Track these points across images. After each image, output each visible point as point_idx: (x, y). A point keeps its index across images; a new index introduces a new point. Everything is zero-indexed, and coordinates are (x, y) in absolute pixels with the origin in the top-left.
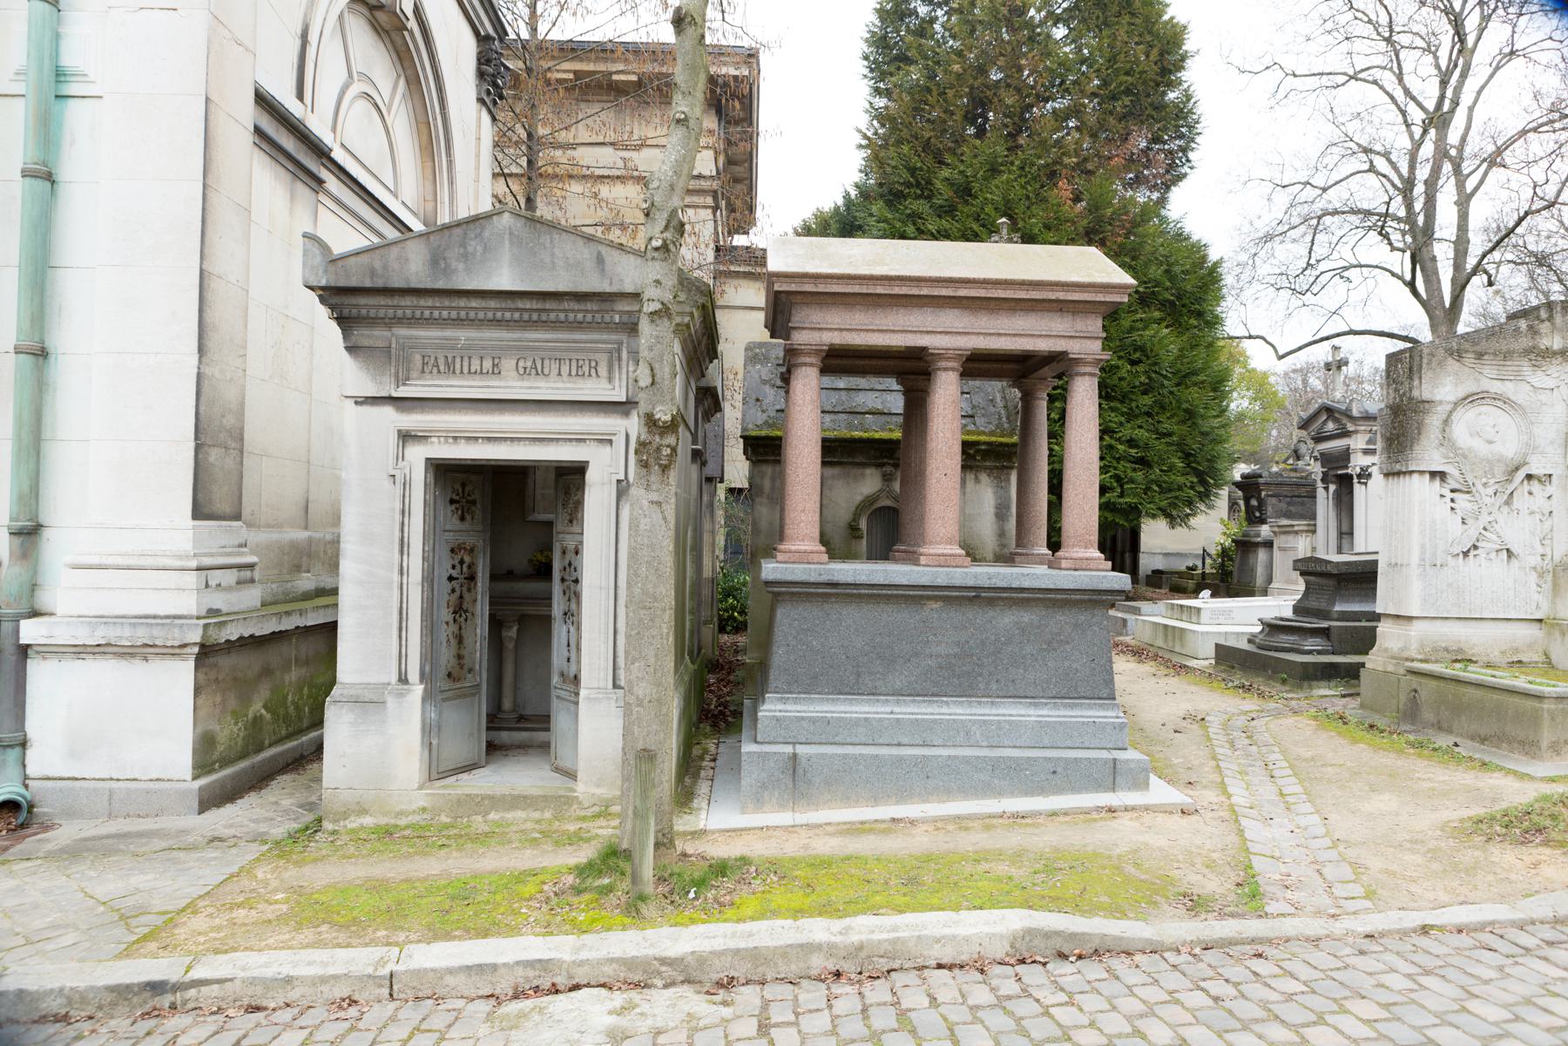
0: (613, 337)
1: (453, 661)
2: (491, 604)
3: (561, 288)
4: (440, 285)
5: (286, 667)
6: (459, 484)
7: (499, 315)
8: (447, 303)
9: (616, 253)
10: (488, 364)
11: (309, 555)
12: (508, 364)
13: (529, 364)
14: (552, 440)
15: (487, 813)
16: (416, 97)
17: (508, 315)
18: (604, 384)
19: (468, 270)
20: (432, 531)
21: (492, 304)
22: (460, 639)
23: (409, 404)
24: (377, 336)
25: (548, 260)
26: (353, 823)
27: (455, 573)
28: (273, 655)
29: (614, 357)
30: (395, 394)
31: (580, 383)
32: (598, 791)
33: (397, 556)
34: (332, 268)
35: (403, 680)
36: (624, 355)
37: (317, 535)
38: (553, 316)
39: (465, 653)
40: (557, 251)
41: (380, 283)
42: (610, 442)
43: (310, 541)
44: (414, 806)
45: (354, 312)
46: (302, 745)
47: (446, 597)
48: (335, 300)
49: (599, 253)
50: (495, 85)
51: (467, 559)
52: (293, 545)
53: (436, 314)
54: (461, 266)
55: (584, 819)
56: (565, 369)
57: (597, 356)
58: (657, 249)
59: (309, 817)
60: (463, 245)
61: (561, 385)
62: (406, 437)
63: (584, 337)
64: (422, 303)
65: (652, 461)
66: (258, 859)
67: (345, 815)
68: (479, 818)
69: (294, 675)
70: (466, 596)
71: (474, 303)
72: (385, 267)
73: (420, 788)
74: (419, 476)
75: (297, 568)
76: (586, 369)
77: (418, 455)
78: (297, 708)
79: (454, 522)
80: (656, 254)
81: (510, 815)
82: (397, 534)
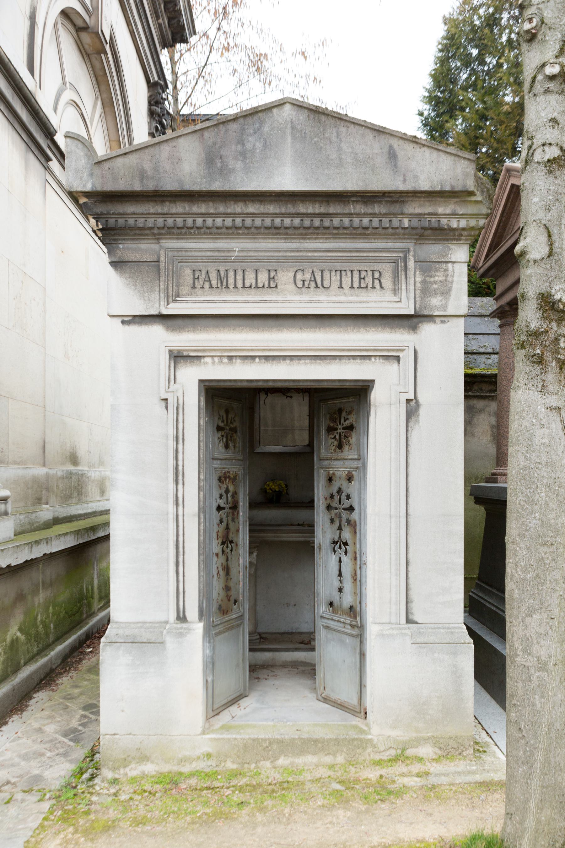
0: (399, 245)
1: (223, 594)
2: (250, 531)
3: (350, 187)
4: (217, 186)
5: (35, 592)
6: (234, 408)
7: (278, 221)
8: (221, 209)
9: (409, 147)
10: (263, 278)
11: (47, 489)
12: (285, 277)
13: (308, 276)
14: (335, 357)
15: (276, 758)
16: (110, 118)
17: (287, 221)
18: (389, 296)
19: (247, 170)
20: (206, 460)
21: (272, 208)
22: (227, 570)
23: (180, 322)
24: (144, 249)
25: (334, 156)
26: (134, 771)
27: (222, 503)
28: (25, 582)
29: (400, 267)
30: (165, 312)
31: (363, 295)
32: (394, 733)
33: (172, 486)
34: (97, 171)
35: (182, 618)
36: (411, 264)
37: (52, 472)
38: (336, 222)
39: (231, 584)
40: (344, 146)
41: (150, 186)
42: (398, 358)
43: (47, 475)
44: (198, 752)
45: (121, 222)
46: (51, 660)
47: (216, 528)
48: (100, 209)
49: (391, 147)
50: (161, 123)
51: (231, 488)
52: (36, 481)
53: (209, 222)
54: (239, 165)
55: (379, 763)
56: (346, 281)
57: (380, 267)
58: (552, 78)
59: (80, 753)
60: (241, 142)
61: (343, 298)
62: (178, 357)
63: (367, 245)
64: (195, 209)
65: (548, 355)
66: (41, 827)
67: (125, 762)
68: (268, 764)
69: (42, 597)
70: (231, 526)
71: (252, 208)
72: (156, 168)
73: (203, 733)
74: (193, 400)
75: (39, 501)
76: (369, 280)
77: (191, 377)
78: (45, 626)
79: (220, 451)
80: (551, 85)
81: (300, 760)
82: (172, 462)
